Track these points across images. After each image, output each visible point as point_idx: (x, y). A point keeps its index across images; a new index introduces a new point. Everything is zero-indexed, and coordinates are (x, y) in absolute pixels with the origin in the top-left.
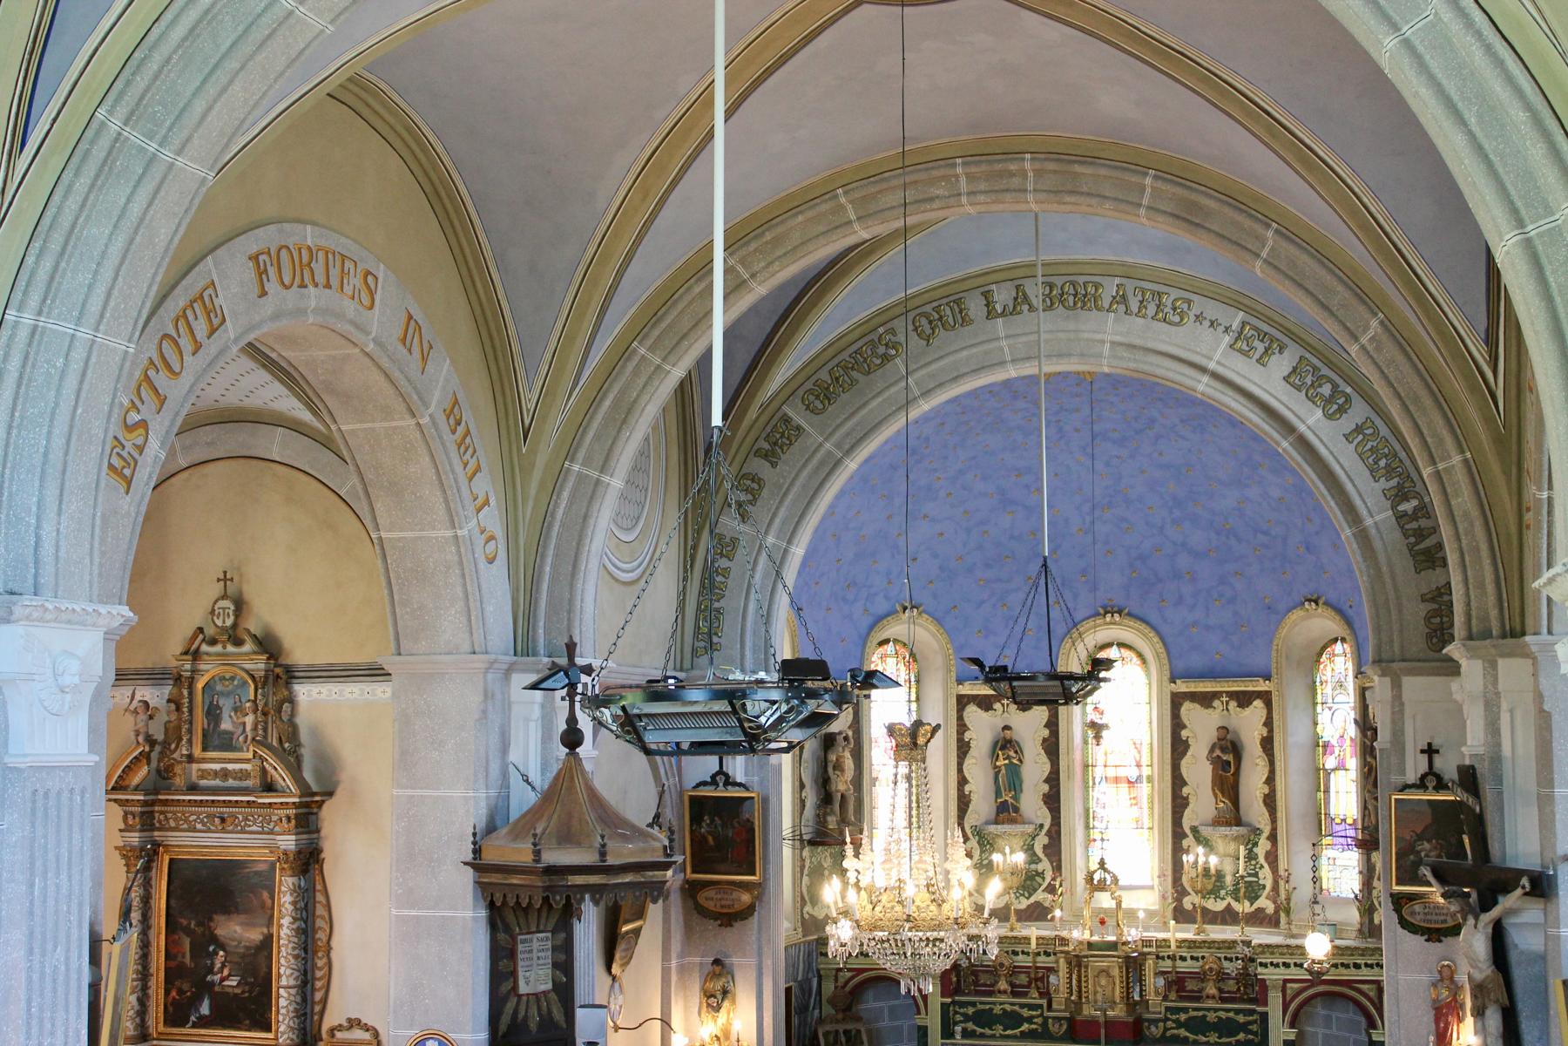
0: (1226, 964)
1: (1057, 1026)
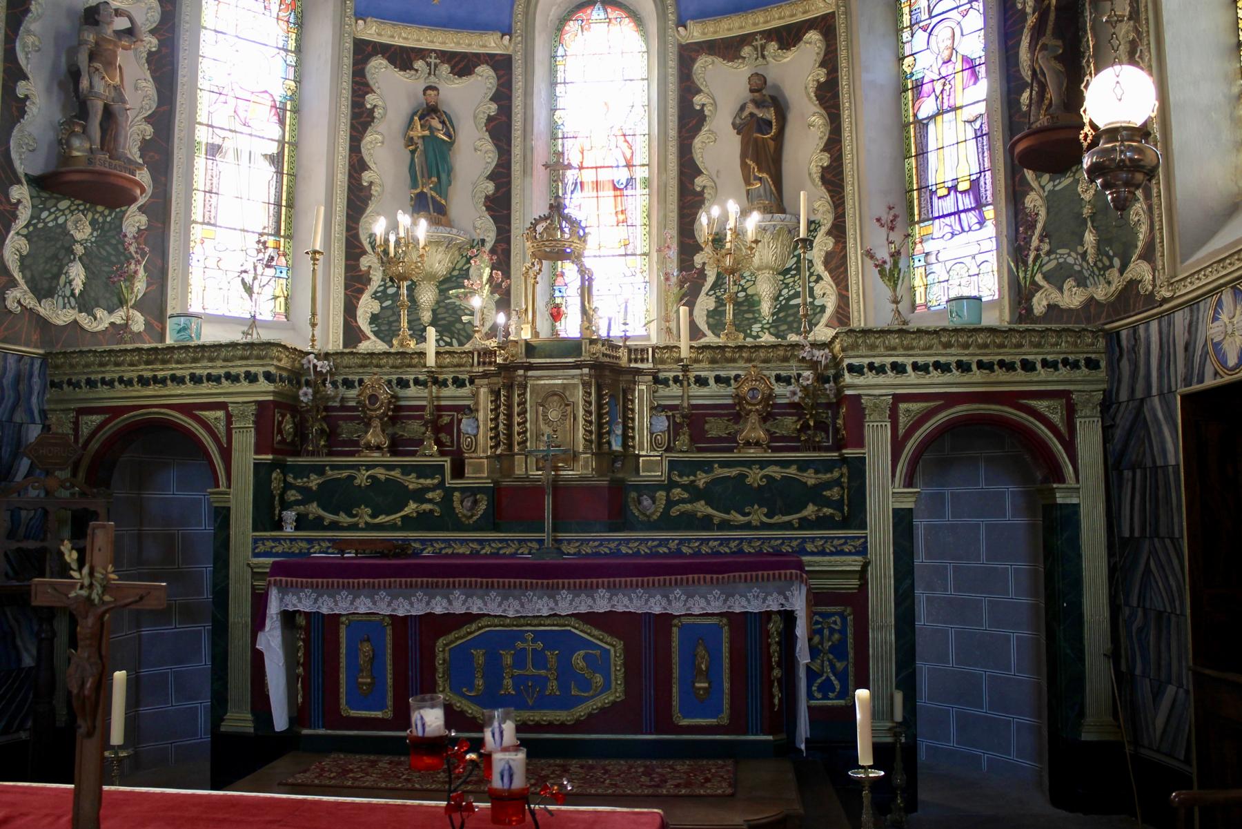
0: (779, 389)
1: (468, 503)
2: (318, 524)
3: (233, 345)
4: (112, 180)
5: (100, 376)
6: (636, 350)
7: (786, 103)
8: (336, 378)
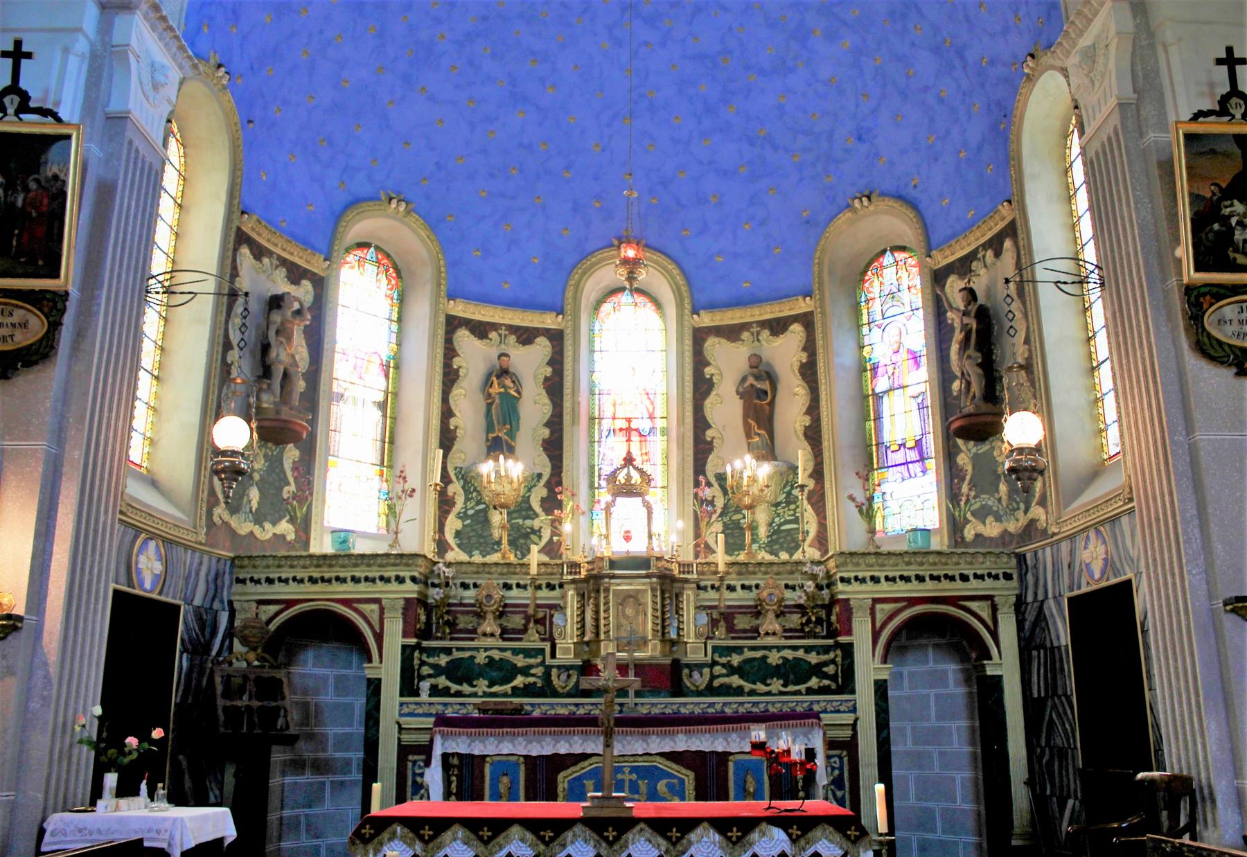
0: (788, 594)
1: (564, 677)
2: (446, 692)
3: (387, 555)
4: (291, 426)
5: (321, 575)
6: (684, 565)
7: (777, 377)
8: (455, 581)
